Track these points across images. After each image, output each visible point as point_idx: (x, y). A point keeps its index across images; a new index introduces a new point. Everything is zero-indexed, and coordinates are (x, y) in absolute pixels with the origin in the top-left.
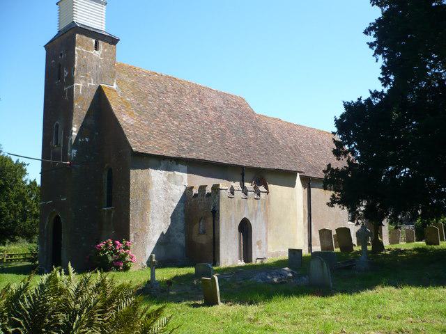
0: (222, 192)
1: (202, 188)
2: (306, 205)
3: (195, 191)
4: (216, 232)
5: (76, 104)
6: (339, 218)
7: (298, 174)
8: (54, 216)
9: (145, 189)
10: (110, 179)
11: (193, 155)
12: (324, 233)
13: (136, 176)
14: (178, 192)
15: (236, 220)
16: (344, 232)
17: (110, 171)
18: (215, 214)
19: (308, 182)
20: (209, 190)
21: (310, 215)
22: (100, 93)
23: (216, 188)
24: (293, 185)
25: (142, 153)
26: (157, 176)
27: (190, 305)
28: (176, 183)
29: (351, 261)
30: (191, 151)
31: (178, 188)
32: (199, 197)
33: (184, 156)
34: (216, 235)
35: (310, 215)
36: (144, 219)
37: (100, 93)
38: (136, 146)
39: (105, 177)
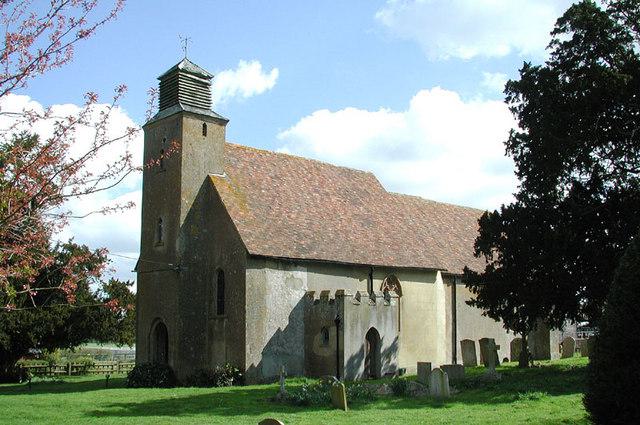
0: (346, 299)
1: (325, 294)
2: (450, 307)
3: (317, 297)
4: (340, 342)
5: (183, 199)
6: (481, 326)
7: (439, 272)
8: (158, 322)
9: (261, 296)
10: (221, 283)
11: (313, 255)
12: (468, 345)
13: (252, 275)
14: (297, 296)
15: (400, 152)
16: (489, 346)
17: (221, 273)
18: (339, 323)
19: (449, 279)
20: (332, 296)
21: (454, 321)
22: (208, 181)
23: (340, 295)
24: (434, 281)
25: (259, 256)
26: (274, 277)
27: (363, 346)
28: (294, 287)
29: (113, 287)
30: (311, 249)
31: (297, 292)
32: (320, 305)
33: (303, 256)
34: (340, 348)
35: (454, 321)
36: (259, 323)
37: (208, 181)
38: (254, 248)
39: (215, 280)
